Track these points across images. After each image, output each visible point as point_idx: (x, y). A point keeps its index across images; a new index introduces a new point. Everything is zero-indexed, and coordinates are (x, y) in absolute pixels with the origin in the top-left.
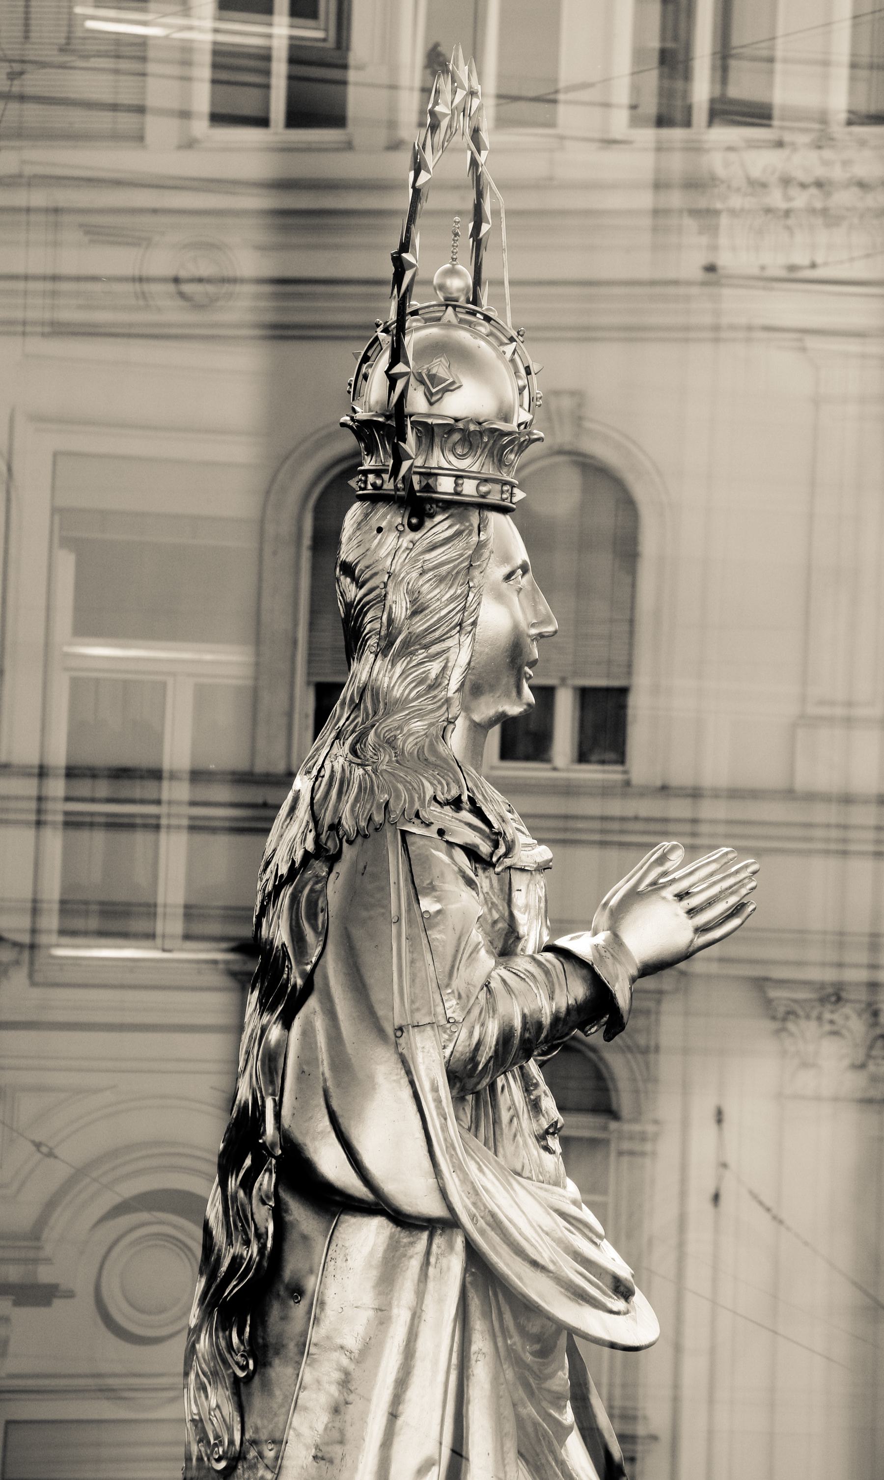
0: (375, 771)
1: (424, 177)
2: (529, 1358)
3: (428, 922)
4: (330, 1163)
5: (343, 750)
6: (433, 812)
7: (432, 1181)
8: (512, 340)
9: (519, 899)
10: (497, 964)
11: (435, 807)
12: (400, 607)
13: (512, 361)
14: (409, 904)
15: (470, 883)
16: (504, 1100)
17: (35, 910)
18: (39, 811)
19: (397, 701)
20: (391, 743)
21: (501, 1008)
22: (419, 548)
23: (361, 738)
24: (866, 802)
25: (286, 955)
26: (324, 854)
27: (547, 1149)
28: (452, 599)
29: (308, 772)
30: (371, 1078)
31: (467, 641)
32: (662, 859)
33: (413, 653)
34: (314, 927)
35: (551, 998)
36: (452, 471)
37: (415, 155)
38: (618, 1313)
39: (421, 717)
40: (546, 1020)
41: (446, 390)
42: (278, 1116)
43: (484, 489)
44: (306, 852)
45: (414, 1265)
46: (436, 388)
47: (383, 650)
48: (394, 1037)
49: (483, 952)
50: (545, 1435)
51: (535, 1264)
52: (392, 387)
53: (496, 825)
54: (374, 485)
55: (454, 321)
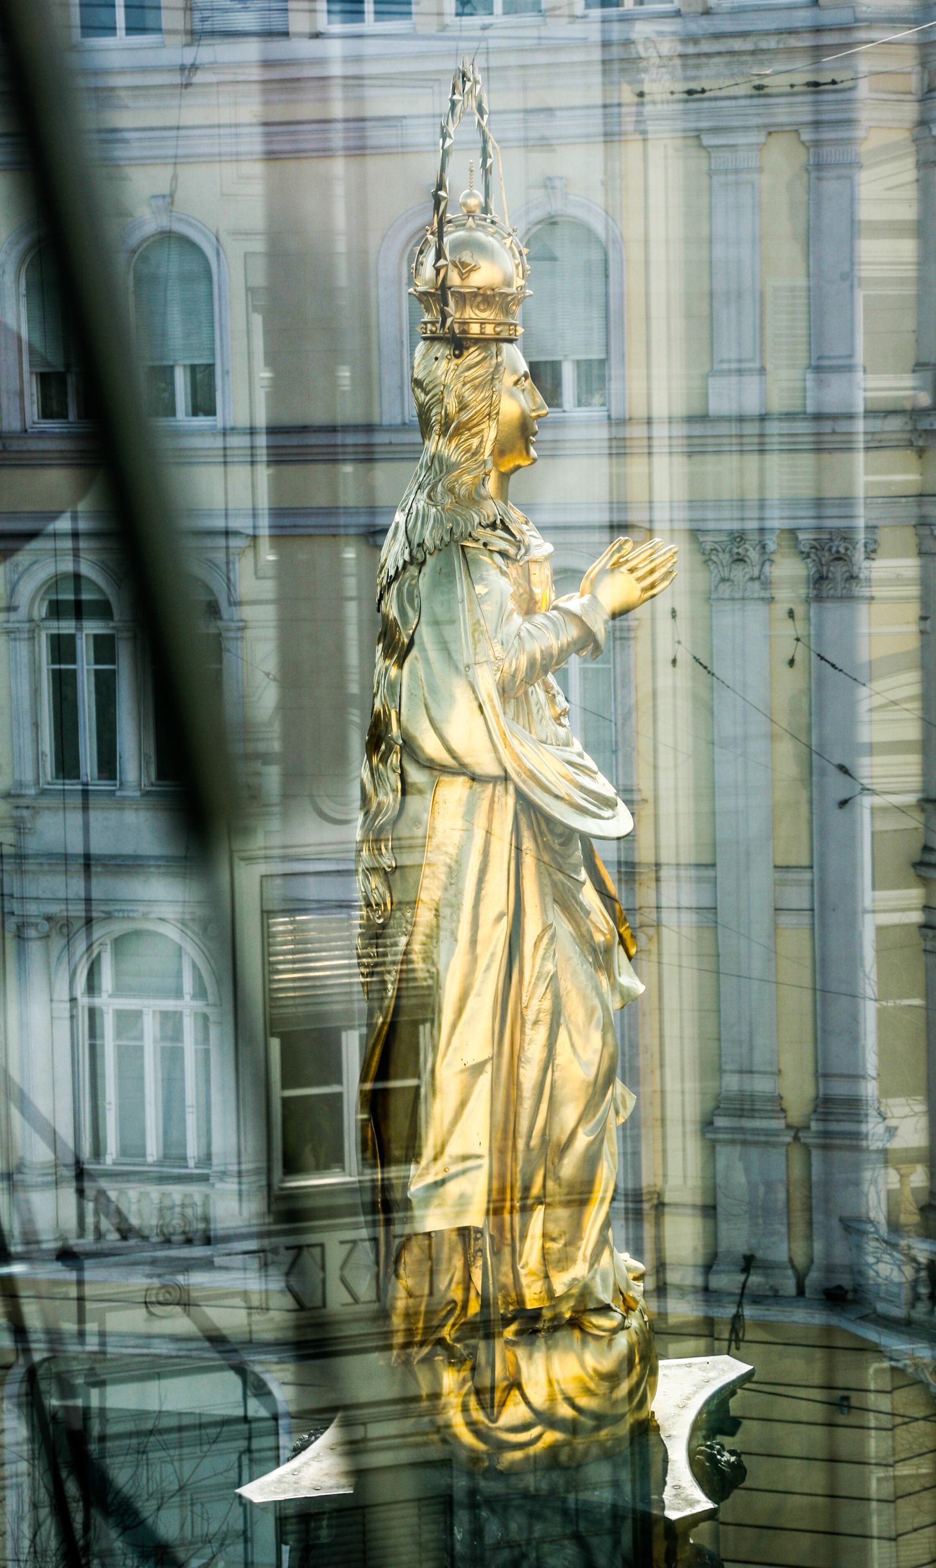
0: (443, 509)
1: (449, 142)
2: (557, 847)
3: (480, 600)
4: (431, 746)
5: (423, 496)
6: (479, 532)
7: (493, 755)
8: (509, 235)
9: (534, 579)
10: (524, 621)
11: (481, 530)
12: (451, 405)
13: (511, 248)
14: (469, 591)
15: (503, 573)
16: (533, 699)
17: (254, 516)
18: (252, 455)
19: (454, 464)
20: (451, 490)
21: (528, 647)
22: (461, 369)
23: (433, 489)
24: (752, 420)
25: (397, 625)
26: (415, 561)
27: (561, 725)
28: (483, 400)
29: (403, 510)
30: (452, 696)
31: (494, 424)
32: (619, 549)
33: (462, 434)
34: (413, 608)
35: (558, 638)
36: (478, 320)
37: (442, 128)
38: (608, 819)
39: (469, 473)
40: (555, 652)
41: (471, 270)
42: (399, 720)
43: (498, 329)
44: (405, 562)
45: (485, 803)
46: (465, 269)
47: (443, 433)
48: (465, 671)
49: (515, 615)
50: (569, 889)
51: (557, 797)
52: (438, 274)
53: (518, 537)
54: (432, 332)
55: (474, 226)
